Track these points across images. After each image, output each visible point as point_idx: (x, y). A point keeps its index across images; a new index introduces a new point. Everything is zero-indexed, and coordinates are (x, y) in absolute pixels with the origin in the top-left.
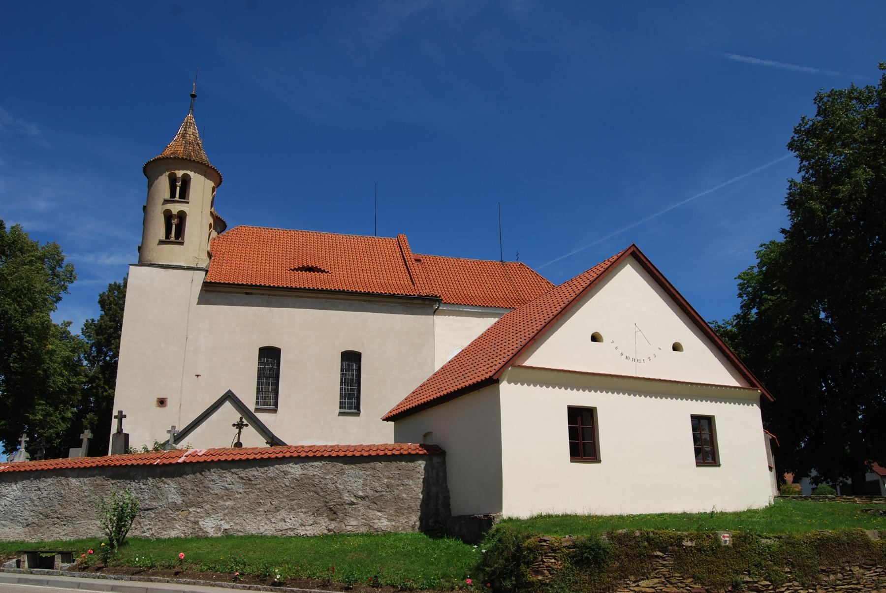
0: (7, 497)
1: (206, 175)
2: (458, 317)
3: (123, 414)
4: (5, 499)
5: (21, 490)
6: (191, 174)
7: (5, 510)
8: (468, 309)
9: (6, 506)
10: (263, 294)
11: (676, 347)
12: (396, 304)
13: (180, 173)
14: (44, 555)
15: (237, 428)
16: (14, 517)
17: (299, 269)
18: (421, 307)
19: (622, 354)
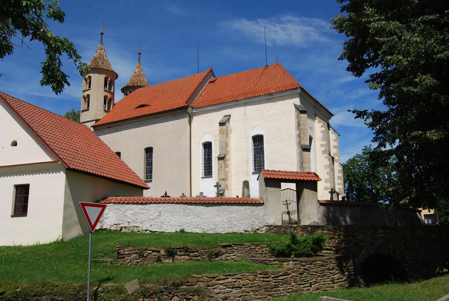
1: (99, 73)
2: (206, 114)
3: (216, 185)
6: (90, 75)
8: (209, 108)
10: (115, 126)
12: (169, 116)
13: (87, 77)
17: (136, 108)
18: (181, 114)
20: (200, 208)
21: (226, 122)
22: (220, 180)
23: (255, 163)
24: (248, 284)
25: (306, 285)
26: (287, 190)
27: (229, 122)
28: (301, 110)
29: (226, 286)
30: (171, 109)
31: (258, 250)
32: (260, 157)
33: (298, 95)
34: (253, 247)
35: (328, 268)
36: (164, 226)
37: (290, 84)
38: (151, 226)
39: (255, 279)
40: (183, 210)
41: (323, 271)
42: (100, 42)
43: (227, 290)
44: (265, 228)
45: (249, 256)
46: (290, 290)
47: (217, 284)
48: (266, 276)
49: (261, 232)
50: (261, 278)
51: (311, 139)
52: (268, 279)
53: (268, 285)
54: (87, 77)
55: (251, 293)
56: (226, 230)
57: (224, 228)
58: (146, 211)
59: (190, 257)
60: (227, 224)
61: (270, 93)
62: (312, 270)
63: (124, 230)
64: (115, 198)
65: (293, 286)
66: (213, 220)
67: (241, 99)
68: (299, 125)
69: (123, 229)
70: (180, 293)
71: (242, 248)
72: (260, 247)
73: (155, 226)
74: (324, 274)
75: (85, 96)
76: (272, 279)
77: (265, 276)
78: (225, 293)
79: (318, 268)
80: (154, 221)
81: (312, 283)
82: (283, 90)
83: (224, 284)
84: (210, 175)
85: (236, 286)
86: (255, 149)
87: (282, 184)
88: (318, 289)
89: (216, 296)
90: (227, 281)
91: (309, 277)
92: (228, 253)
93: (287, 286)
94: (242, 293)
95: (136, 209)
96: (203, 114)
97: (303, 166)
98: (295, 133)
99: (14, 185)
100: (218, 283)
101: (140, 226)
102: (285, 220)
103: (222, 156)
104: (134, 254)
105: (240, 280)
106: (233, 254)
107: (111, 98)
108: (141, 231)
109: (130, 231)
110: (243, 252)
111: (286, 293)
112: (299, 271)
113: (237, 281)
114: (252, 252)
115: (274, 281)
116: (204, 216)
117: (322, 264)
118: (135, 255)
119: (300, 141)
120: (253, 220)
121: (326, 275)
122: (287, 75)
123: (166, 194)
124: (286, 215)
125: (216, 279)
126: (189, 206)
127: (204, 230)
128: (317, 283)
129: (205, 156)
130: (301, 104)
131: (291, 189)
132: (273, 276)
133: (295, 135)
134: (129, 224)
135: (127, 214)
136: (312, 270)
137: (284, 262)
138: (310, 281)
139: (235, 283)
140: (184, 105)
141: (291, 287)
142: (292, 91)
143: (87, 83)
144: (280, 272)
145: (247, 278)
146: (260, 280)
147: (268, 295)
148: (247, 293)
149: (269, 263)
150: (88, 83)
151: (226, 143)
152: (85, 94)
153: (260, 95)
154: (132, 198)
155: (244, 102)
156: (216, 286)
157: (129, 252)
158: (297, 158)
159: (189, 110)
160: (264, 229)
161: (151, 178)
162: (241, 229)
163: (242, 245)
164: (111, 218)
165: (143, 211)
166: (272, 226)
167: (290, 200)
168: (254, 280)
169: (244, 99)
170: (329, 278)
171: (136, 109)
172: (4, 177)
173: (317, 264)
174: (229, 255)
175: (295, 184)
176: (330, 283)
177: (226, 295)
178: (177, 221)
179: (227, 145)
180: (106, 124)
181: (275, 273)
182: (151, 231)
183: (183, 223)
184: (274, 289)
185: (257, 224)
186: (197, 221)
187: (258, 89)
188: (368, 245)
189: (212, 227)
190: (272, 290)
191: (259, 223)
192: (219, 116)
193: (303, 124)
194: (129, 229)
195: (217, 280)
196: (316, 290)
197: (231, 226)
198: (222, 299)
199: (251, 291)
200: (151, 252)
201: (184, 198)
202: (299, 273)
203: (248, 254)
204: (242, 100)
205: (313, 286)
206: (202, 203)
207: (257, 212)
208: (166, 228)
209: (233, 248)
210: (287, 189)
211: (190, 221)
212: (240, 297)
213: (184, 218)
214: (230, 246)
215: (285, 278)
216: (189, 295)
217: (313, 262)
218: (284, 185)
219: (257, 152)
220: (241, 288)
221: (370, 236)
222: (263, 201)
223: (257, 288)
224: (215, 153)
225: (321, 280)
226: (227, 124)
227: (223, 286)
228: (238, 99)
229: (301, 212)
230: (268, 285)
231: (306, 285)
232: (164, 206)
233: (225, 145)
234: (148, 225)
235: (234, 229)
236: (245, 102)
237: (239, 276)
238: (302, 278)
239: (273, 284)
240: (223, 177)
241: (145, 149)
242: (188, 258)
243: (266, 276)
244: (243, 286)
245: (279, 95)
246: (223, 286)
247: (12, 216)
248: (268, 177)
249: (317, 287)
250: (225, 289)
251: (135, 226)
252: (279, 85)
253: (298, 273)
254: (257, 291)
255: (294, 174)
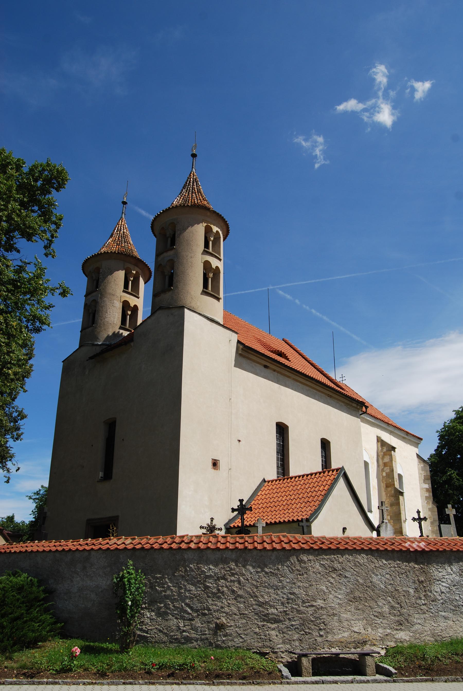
0: (443, 582)
4: (440, 584)
5: (458, 574)
7: (442, 599)
8: (368, 417)
9: (442, 592)
10: (274, 371)
15: (208, 525)
16: (455, 606)
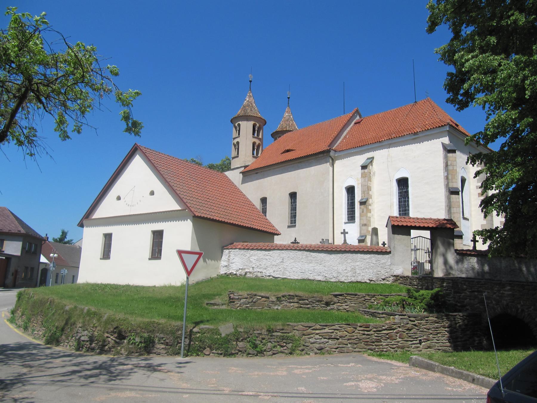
6: (239, 122)
10: (262, 172)
11: (152, 193)
12: (313, 160)
14: (519, 391)
17: (282, 153)
19: (127, 204)
20: (323, 256)
21: (369, 164)
22: (361, 225)
23: (399, 208)
24: (346, 336)
25: (414, 342)
26: (418, 238)
27: (372, 165)
28: (449, 149)
29: (322, 336)
30: (314, 153)
31: (373, 301)
32: (405, 201)
33: (447, 133)
34: (367, 297)
35: (443, 325)
36: (287, 272)
37: (438, 121)
38: (274, 272)
39: (354, 332)
40: (305, 257)
41: (437, 328)
42: (249, 89)
43: (323, 340)
44: (392, 278)
45: (363, 307)
46: (395, 346)
47: (312, 334)
48: (367, 329)
49: (387, 283)
50: (362, 331)
51: (463, 181)
52: (369, 333)
53: (369, 338)
54: (236, 125)
55: (349, 345)
56: (349, 278)
57: (347, 276)
58: (269, 257)
59: (299, 305)
60: (351, 273)
61: (415, 132)
62: (423, 327)
63: (248, 275)
64: (242, 243)
65: (398, 342)
66: (336, 268)
67: (385, 140)
68: (447, 165)
69: (248, 273)
70: (273, 340)
71: (355, 298)
72: (376, 298)
73: (278, 272)
74: (438, 331)
75: (235, 143)
76: (373, 333)
77: (365, 329)
78: (320, 343)
79: (431, 324)
80: (277, 267)
81: (422, 341)
82: (430, 128)
83: (320, 334)
84: (353, 220)
85: (333, 337)
86: (400, 193)
87: (412, 231)
88: (429, 347)
89: (311, 346)
90: (323, 331)
91: (418, 334)
92: (340, 303)
93: (391, 341)
94: (339, 345)
95: (260, 255)
96: (351, 157)
97: (451, 211)
98: (443, 174)
99: (103, 234)
100: (314, 333)
101: (264, 271)
102: (428, 269)
103: (364, 200)
104: (243, 298)
105: (338, 332)
106: (346, 304)
107: (259, 144)
108: (264, 276)
109: (254, 276)
110: (356, 303)
111: (389, 348)
112: (406, 327)
113: (334, 332)
114: (367, 303)
115: (376, 335)
116: (327, 264)
117: (436, 320)
118: (245, 300)
119: (448, 183)
120: (379, 269)
121: (441, 333)
122: (436, 111)
123: (295, 240)
124: (428, 264)
125: (312, 328)
126: (312, 253)
127: (326, 278)
128: (428, 340)
129: (348, 200)
130: (451, 142)
131: (423, 237)
132: (375, 329)
133: (443, 177)
134: (253, 269)
135: (251, 260)
136: (423, 327)
137: (391, 316)
138: (420, 338)
139: (332, 334)
140: (326, 148)
141: (396, 343)
142: (442, 128)
143: (236, 131)
144: (383, 326)
145: (345, 330)
146: (359, 333)
147: (369, 349)
148: (345, 345)
149: (378, 316)
150: (238, 131)
151: (368, 187)
152: (235, 141)
153: (404, 135)
154: (258, 244)
155: (387, 143)
156: (312, 336)
157: (239, 296)
158: (445, 202)
159: (332, 153)
160: (391, 279)
161: (295, 223)
162: (366, 279)
163: (356, 295)
164: (237, 263)
165: (267, 257)
166: (398, 276)
167: (424, 249)
168: (353, 333)
169: (387, 139)
170: (444, 337)
171: (281, 154)
172: (168, 222)
173: (430, 320)
174: (341, 305)
175: (429, 232)
176: (445, 342)
177: (322, 345)
178: (299, 268)
179: (369, 189)
180: (253, 170)
181: (377, 327)
182: (274, 277)
183: (306, 270)
184: (375, 343)
185: (383, 273)
186: (319, 268)
187: (403, 128)
188: (494, 302)
189: (335, 275)
190: (374, 344)
191: (385, 272)
192: (361, 159)
193: (451, 165)
194: (254, 274)
195: (313, 330)
196: (427, 349)
197: (354, 275)
198: (317, 349)
199: (349, 343)
200: (260, 298)
201: (296, 245)
202: (406, 328)
203: (362, 305)
204: (385, 141)
205: (423, 344)
206: (329, 251)
207: (383, 261)
208: (289, 275)
209: (346, 298)
210: (419, 237)
211: (313, 268)
212: (336, 349)
213: (306, 265)
214: (341, 295)
215: (389, 333)
216: (282, 342)
217: (424, 318)
218: (414, 233)
219: (402, 196)
220: (338, 339)
221: (496, 293)
222: (391, 249)
223: (356, 341)
224: (358, 197)
225: (434, 338)
226: (369, 166)
227: (318, 336)
228: (381, 140)
229: (435, 262)
230: (369, 338)
231: (414, 342)
232: (287, 253)
233: (367, 189)
234: (271, 271)
235: (358, 278)
236: (389, 143)
237: (337, 327)
238: (409, 335)
239: (375, 338)
240: (365, 222)
241: (289, 194)
242: (297, 306)
243: (367, 329)
244: (340, 337)
245: (426, 134)
246: (319, 336)
247: (149, 259)
248: (396, 224)
249: (428, 345)
250: (321, 339)
251: (258, 272)
252: (427, 122)
253: (405, 328)
254: (356, 344)
255: (426, 221)
